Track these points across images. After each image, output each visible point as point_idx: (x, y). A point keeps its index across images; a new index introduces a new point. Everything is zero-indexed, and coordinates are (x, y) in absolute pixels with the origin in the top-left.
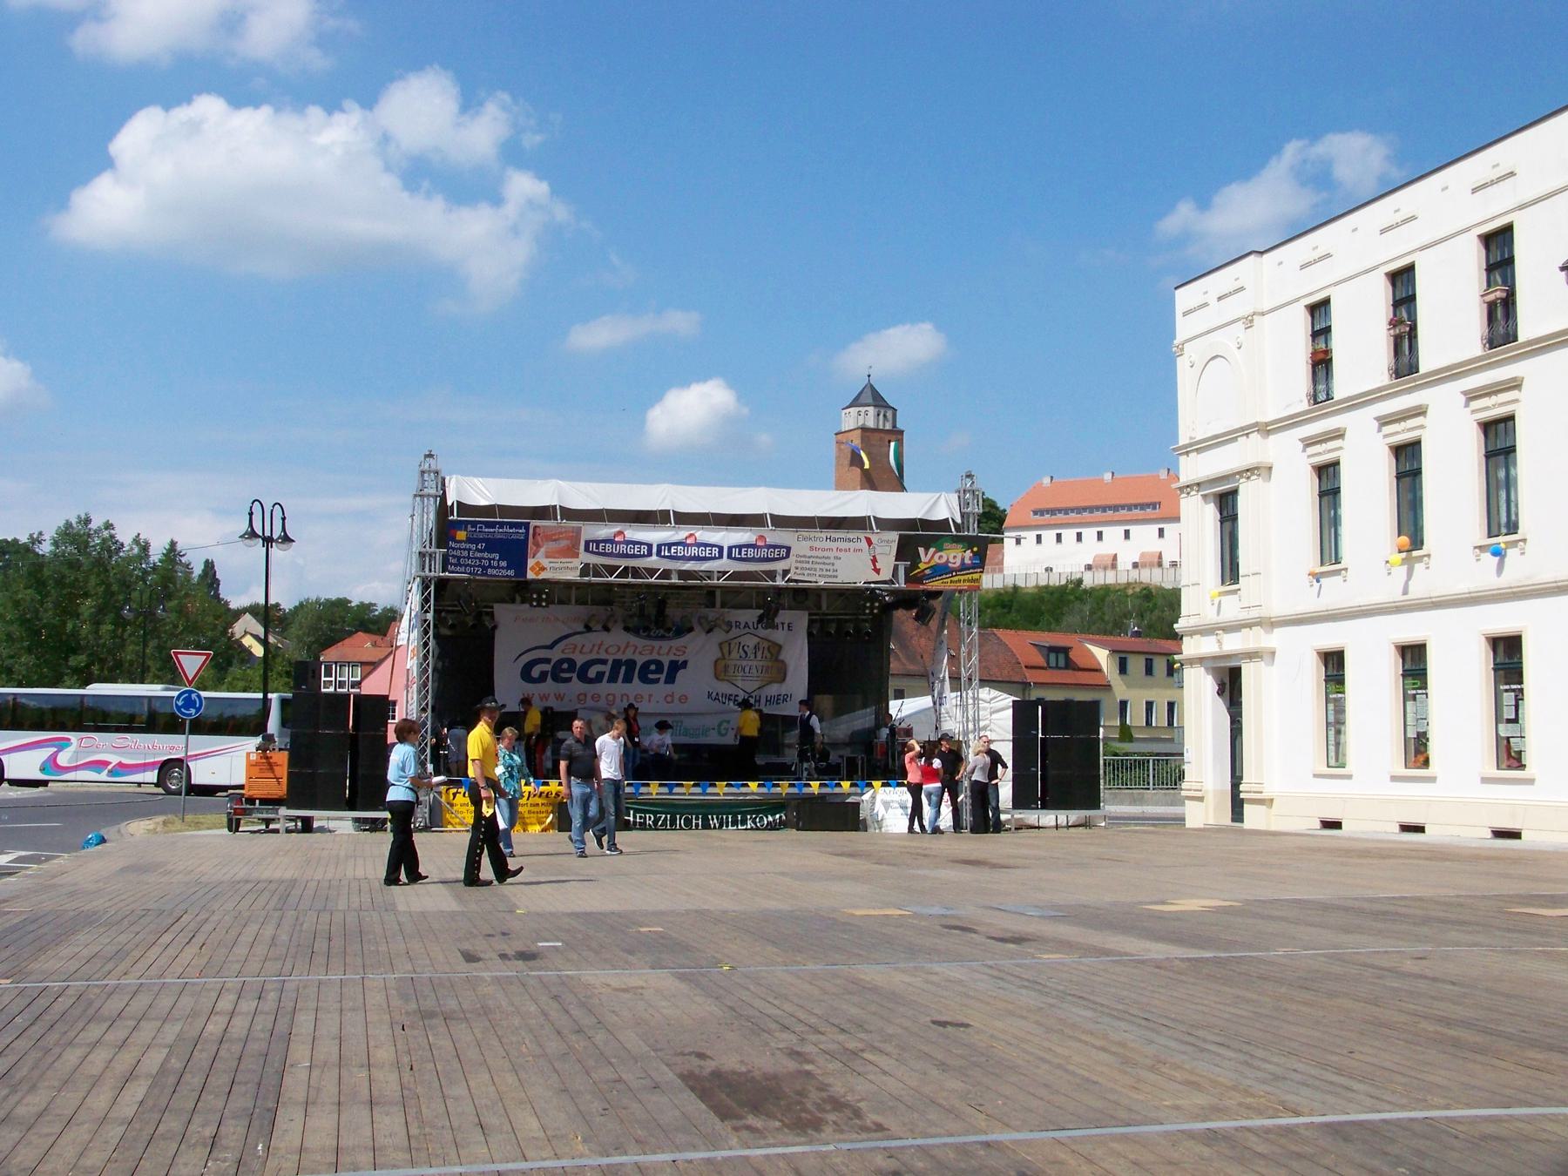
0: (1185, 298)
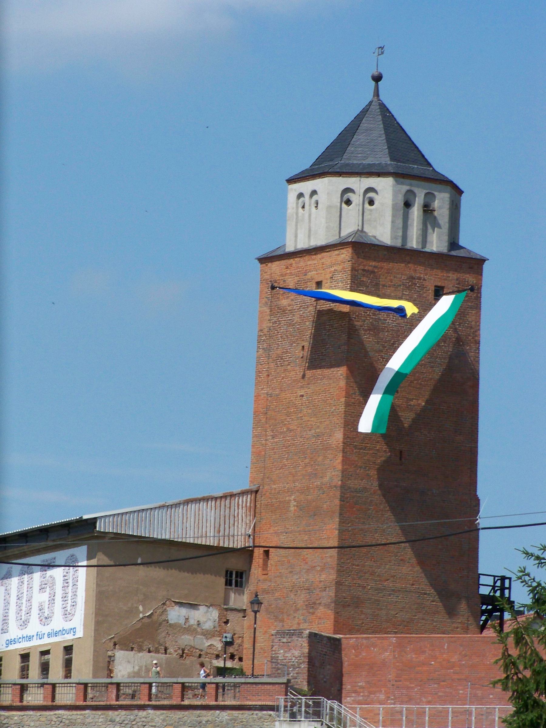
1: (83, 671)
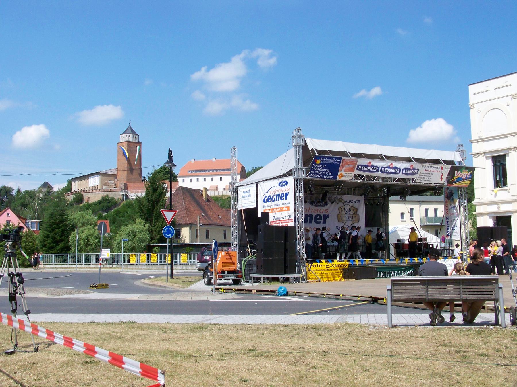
0: (472, 89)
1: (99, 188)
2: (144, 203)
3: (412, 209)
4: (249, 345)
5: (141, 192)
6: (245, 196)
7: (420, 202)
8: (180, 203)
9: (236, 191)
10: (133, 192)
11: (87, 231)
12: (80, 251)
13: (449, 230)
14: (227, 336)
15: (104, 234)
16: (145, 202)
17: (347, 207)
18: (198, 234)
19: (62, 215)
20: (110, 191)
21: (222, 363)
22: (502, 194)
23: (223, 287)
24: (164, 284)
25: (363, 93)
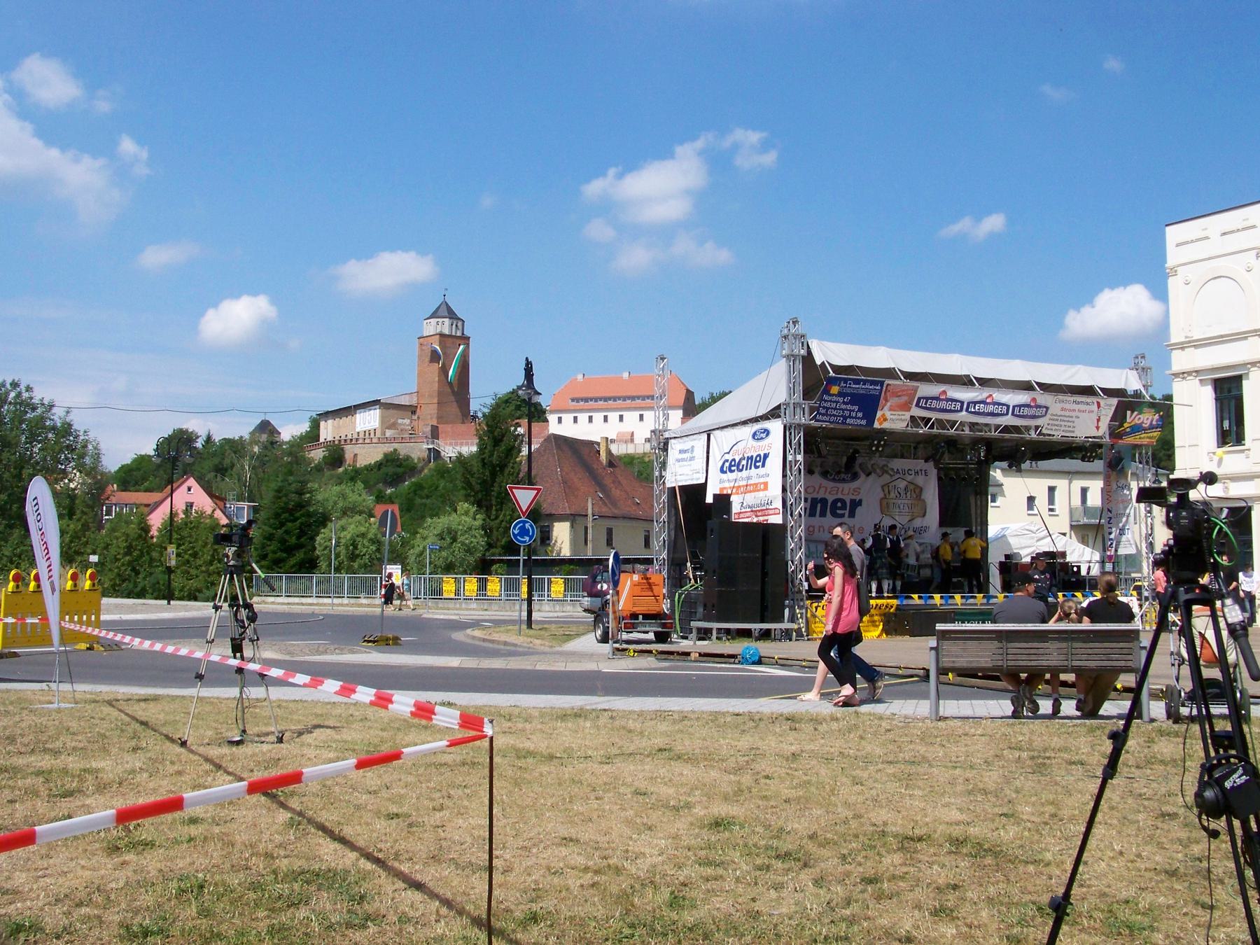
0: (1174, 234)
1: (378, 434)
2: (475, 469)
3: (1052, 490)
4: (659, 742)
5: (467, 444)
6: (683, 460)
7: (1069, 473)
8: (552, 471)
9: (665, 449)
10: (451, 444)
11: (353, 526)
12: (338, 570)
13: (1112, 536)
14: (624, 728)
15: (391, 535)
16: (476, 466)
17: (902, 485)
18: (590, 537)
19: (300, 493)
20: (402, 441)
21: (606, 767)
22: (1230, 462)
23: (632, 647)
24: (512, 638)
25: (964, 224)
